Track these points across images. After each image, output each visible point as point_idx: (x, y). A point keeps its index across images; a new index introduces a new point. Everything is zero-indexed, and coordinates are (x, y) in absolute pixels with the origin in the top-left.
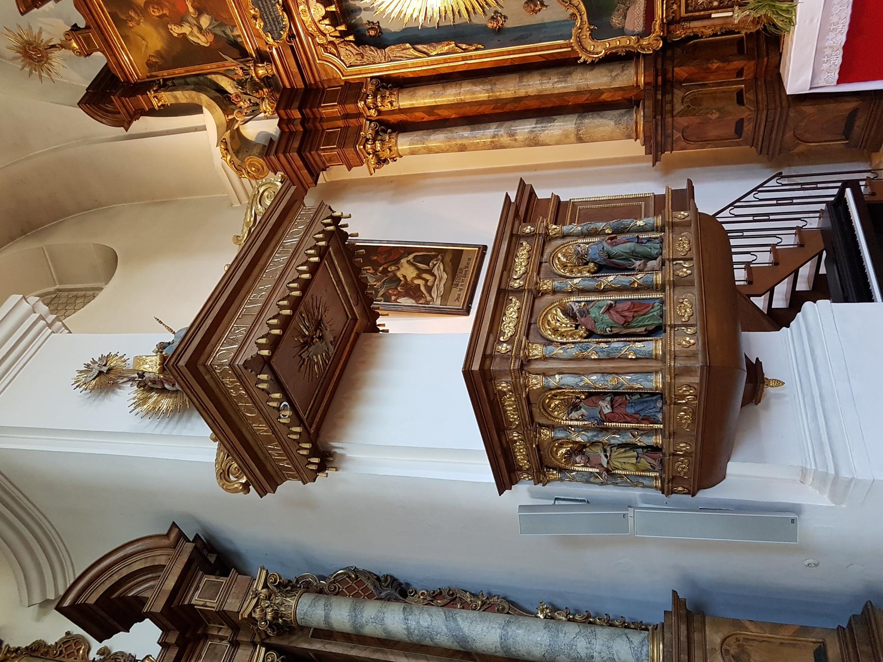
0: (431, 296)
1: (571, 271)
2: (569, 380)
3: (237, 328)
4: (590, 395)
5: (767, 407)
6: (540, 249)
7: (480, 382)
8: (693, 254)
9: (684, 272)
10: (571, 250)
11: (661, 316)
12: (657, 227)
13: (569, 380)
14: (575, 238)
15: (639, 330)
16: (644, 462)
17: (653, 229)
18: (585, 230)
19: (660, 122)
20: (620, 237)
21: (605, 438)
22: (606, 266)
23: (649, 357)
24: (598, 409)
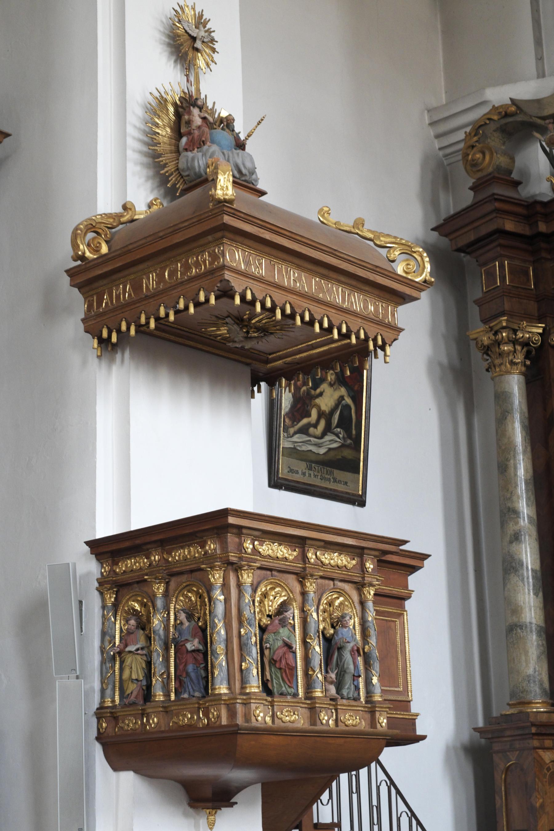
0: (295, 433)
1: (324, 611)
2: (220, 609)
3: (261, 266)
4: (204, 630)
5: (186, 815)
6: (347, 578)
7: (216, 524)
8: (342, 727)
9: (324, 717)
10: (348, 611)
11: (282, 694)
12: (371, 697)
13: (220, 609)
14: (360, 614)
15: (268, 674)
16: (132, 688)
17: (369, 693)
18: (368, 624)
19: (527, 731)
20: (360, 660)
21: (157, 647)
22: (331, 645)
23: (244, 682)
24: (190, 638)
